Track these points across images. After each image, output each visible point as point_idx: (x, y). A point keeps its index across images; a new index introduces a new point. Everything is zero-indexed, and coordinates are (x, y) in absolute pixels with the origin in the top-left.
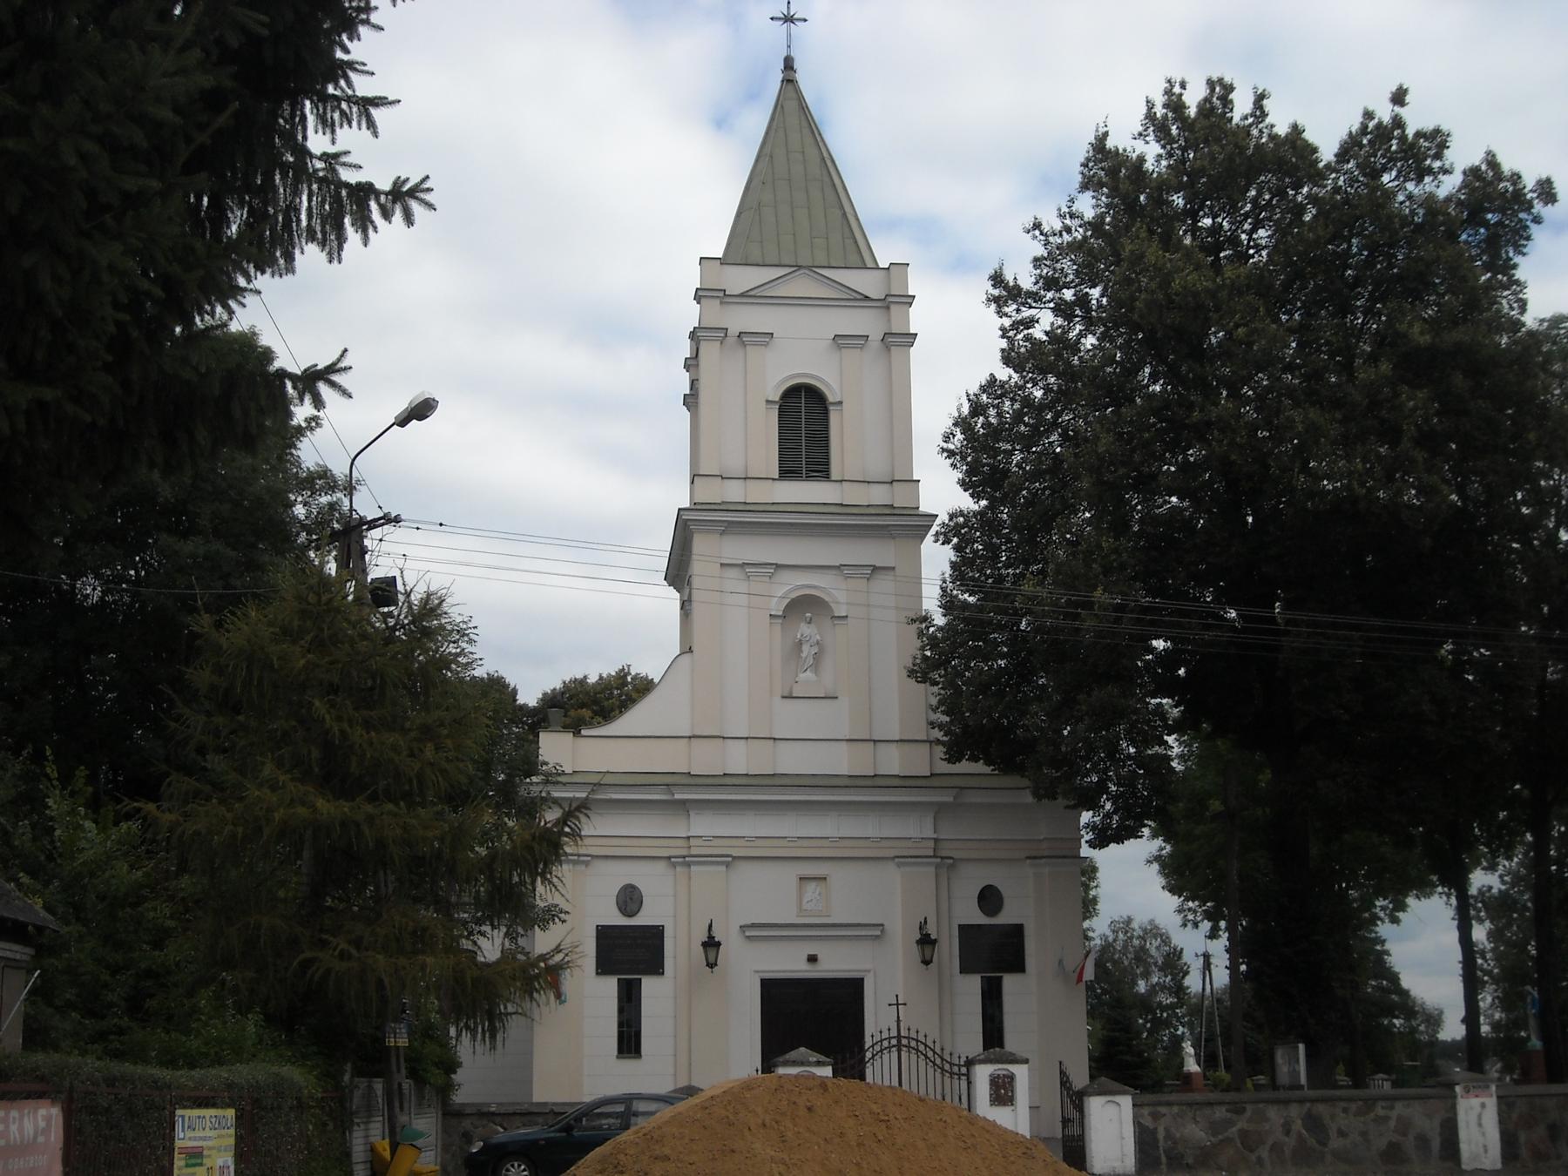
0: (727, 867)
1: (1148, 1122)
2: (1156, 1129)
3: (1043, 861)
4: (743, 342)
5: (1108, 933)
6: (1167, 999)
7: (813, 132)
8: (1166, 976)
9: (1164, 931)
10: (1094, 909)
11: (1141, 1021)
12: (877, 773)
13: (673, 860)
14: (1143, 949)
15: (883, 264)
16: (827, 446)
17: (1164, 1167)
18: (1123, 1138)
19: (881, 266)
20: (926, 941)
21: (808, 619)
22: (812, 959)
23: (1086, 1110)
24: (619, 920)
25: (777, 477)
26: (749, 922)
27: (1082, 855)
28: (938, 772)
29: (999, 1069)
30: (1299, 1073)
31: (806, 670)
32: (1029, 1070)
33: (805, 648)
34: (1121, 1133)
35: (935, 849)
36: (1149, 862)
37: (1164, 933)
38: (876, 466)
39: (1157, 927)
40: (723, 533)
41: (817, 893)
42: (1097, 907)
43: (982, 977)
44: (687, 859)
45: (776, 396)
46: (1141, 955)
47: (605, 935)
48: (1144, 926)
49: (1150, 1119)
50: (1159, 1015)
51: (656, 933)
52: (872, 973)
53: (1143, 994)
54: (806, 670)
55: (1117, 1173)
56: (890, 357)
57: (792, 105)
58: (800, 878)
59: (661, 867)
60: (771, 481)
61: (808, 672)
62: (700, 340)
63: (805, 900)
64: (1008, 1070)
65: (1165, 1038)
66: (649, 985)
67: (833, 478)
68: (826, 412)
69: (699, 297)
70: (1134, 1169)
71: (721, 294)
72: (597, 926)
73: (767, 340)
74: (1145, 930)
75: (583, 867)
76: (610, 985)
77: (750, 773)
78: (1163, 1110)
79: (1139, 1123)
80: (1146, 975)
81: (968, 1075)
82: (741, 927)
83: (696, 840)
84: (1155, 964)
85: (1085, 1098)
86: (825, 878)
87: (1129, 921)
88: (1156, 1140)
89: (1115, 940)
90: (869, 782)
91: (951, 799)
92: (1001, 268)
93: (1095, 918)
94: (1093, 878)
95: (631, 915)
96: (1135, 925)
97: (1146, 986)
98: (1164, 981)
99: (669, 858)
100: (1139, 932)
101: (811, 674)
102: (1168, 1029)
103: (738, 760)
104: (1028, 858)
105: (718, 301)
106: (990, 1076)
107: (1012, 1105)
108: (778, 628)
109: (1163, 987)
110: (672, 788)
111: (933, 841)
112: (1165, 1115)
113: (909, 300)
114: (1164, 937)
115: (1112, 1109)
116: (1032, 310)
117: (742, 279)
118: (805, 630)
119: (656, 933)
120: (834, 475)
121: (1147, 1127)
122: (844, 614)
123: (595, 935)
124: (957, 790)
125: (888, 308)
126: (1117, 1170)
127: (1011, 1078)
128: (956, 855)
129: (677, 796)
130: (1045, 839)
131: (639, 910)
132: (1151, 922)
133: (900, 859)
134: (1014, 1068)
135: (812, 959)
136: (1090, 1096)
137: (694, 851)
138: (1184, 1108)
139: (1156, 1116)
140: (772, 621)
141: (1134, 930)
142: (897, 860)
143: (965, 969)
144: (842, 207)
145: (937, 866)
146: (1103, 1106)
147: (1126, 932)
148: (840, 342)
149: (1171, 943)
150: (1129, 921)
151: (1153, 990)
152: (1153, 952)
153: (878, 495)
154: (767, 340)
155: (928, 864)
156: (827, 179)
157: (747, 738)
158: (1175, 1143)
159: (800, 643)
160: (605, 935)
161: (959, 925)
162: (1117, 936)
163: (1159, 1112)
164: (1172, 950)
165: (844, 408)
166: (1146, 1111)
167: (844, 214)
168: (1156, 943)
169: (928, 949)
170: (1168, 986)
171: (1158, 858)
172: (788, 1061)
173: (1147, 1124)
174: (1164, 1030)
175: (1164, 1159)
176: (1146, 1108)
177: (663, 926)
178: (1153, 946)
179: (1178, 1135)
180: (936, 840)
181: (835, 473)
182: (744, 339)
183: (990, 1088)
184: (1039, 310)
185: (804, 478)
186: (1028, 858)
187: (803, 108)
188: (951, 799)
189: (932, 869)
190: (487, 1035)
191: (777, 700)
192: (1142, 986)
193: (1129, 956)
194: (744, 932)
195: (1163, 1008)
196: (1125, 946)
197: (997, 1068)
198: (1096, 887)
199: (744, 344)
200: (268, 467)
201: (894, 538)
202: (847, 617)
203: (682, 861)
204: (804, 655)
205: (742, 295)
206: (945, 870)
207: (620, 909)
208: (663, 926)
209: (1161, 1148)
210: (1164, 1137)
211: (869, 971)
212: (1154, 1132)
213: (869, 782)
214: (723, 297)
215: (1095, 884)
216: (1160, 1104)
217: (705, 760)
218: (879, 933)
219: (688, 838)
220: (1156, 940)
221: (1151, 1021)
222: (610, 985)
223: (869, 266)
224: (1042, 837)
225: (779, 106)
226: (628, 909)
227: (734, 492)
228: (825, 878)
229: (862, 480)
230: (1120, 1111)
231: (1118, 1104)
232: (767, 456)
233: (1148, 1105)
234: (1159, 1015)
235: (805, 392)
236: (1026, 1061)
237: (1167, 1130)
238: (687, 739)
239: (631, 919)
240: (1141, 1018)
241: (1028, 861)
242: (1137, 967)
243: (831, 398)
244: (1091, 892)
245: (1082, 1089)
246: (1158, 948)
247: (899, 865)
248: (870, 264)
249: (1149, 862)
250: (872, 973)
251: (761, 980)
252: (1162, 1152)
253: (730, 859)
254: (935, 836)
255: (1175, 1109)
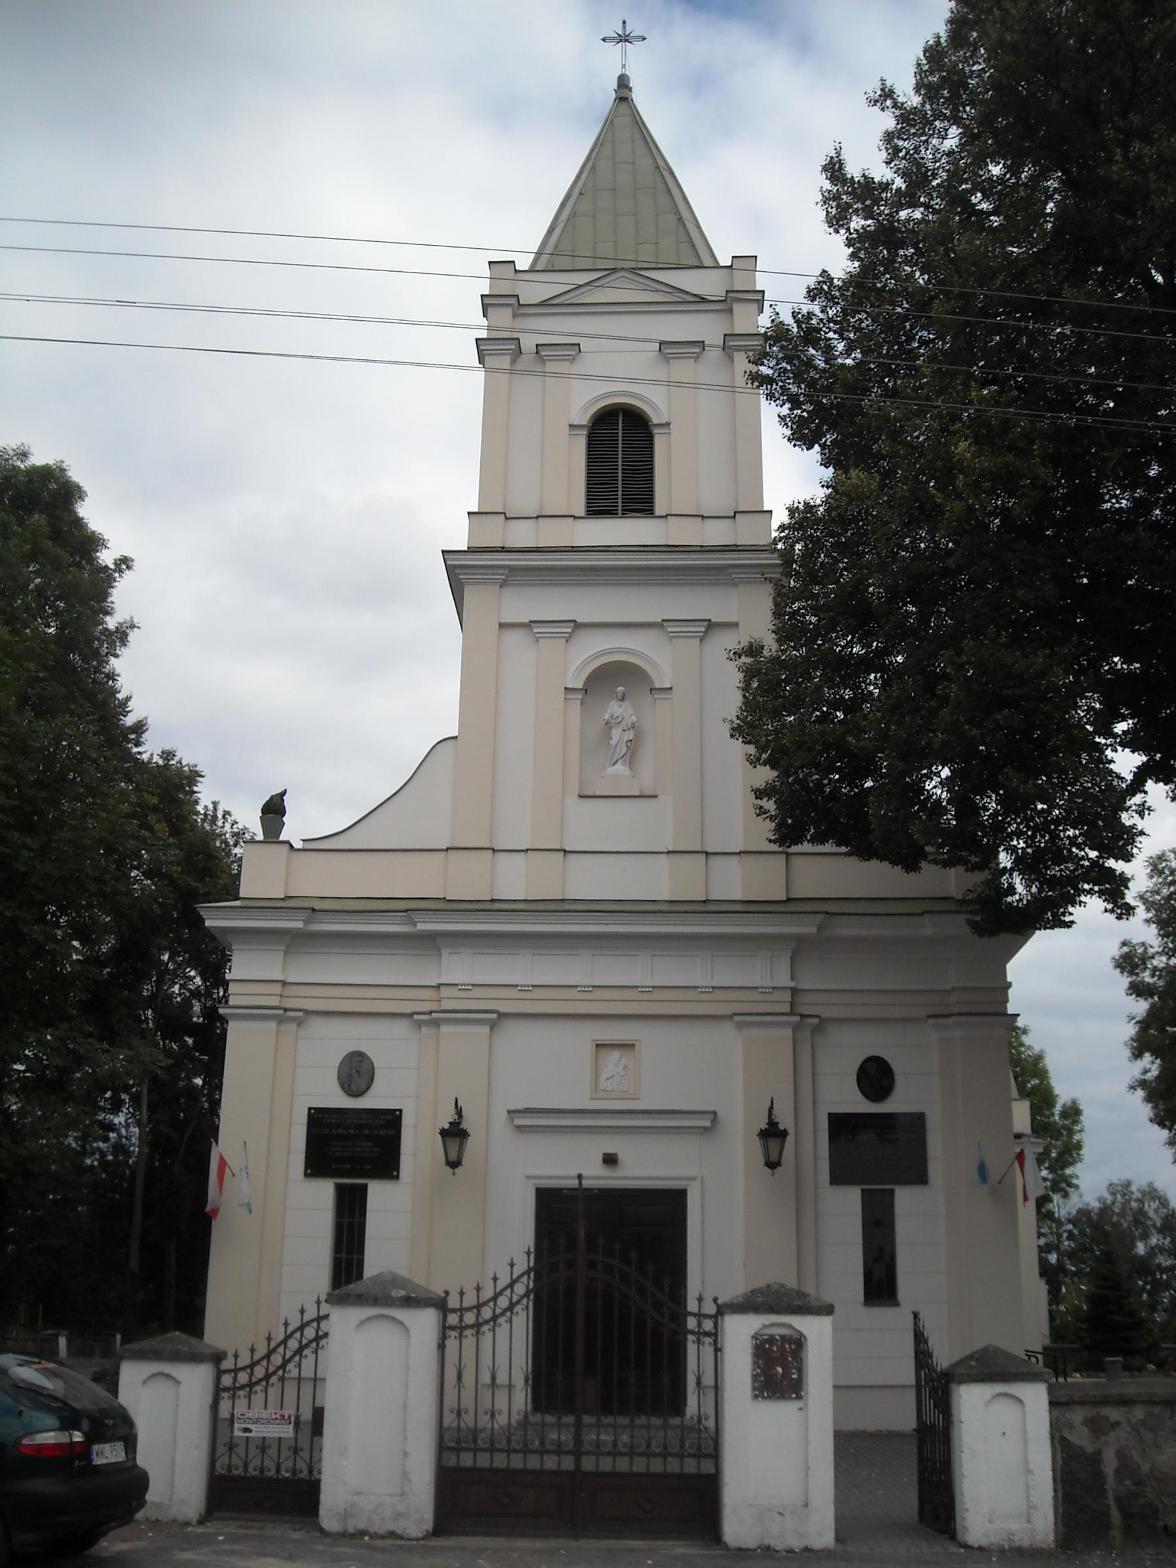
0: (491, 1028)
1: (1081, 1437)
2: (1099, 1452)
3: (951, 1021)
4: (541, 356)
5: (1107, 1195)
6: (1166, 1261)
7: (647, 144)
8: (1165, 1238)
9: (1162, 1193)
10: (1078, 1154)
11: (1140, 1283)
12: (709, 898)
13: (415, 1017)
14: (1141, 1212)
15: (725, 261)
16: (651, 480)
17: (1116, 1534)
18: (1029, 1472)
19: (722, 265)
20: (772, 1133)
21: (620, 695)
22: (610, 1160)
23: (954, 1411)
24: (339, 1100)
25: (582, 513)
26: (521, 1106)
27: (1010, 1012)
28: (796, 897)
29: (773, 1325)
30: (1090, 1382)
31: (616, 762)
32: (835, 1330)
33: (616, 734)
34: (1026, 1461)
35: (792, 1004)
36: (1133, 1088)
37: (1162, 1196)
38: (715, 499)
39: (1155, 1190)
40: (503, 584)
41: (622, 1066)
42: (1082, 1152)
43: (862, 1190)
44: (434, 1015)
45: (585, 419)
46: (1139, 1217)
47: (319, 1120)
48: (1142, 1188)
49: (1085, 1431)
50: (1158, 1277)
51: (391, 1120)
52: (699, 1180)
53: (1142, 1256)
54: (616, 762)
55: (1018, 1543)
56: (733, 366)
57: (624, 121)
58: (597, 1045)
59: (401, 1028)
60: (572, 518)
61: (618, 765)
62: (485, 355)
63: (604, 1076)
64: (790, 1327)
65: (1165, 1300)
66: (378, 1192)
67: (657, 514)
68: (651, 437)
69: (488, 303)
70: (1052, 1537)
71: (513, 301)
72: (310, 1109)
73: (572, 353)
74: (1144, 1193)
75: (293, 1026)
76: (324, 1191)
77: (528, 899)
78: (1113, 1413)
79: (1063, 1440)
80: (1145, 1237)
81: (715, 1335)
82: (509, 1112)
83: (453, 992)
84: (1154, 1226)
85: (954, 1387)
86: (633, 1045)
87: (1128, 1184)
88: (1099, 1476)
89: (1113, 1203)
90: (702, 908)
91: (814, 930)
92: (838, 154)
93: (1079, 1164)
94: (1076, 1122)
96: (1134, 1188)
97: (1145, 1248)
98: (1164, 1244)
99: (412, 1014)
100: (1137, 1195)
101: (622, 767)
102: (1169, 1291)
104: (930, 1016)
105: (509, 311)
106: (755, 1337)
107: (799, 1397)
108: (575, 707)
109: (1162, 1249)
110: (414, 915)
111: (790, 992)
112: (1117, 1424)
113: (759, 297)
114: (1162, 1200)
115: (1005, 1412)
118: (615, 708)
119: (391, 1120)
120: (659, 509)
121: (1081, 1448)
122: (668, 686)
123: (305, 1121)
124: (823, 916)
125: (731, 311)
126: (1016, 1539)
127: (798, 1343)
128: (826, 1013)
129: (420, 927)
130: (954, 989)
131: (368, 1088)
132: (1150, 1184)
133: (739, 1019)
134: (802, 1323)
135: (610, 1160)
136: (960, 1383)
137: (446, 1005)
138: (1157, 1410)
139: (1097, 1427)
140: (569, 696)
141: (1132, 1193)
142: (736, 1018)
143: (837, 1179)
144: (677, 212)
145: (796, 1029)
146: (986, 1405)
147: (1125, 1194)
148: (667, 351)
149: (1168, 1205)
150: (1128, 1184)
151: (1153, 1251)
152: (1152, 1214)
153: (716, 534)
154: (572, 353)
155: (786, 1024)
156: (661, 186)
157: (527, 850)
158: (1139, 1483)
160: (319, 1120)
161: (829, 1114)
162: (1115, 1199)
163: (1107, 1418)
164: (1170, 1212)
165: (672, 432)
166: (1077, 1416)
167: (680, 219)
168: (1155, 1205)
169: (774, 1145)
170: (1167, 1248)
171: (1143, 1084)
172: (348, 1295)
173: (1079, 1443)
174: (1165, 1292)
175: (1116, 1516)
176: (1078, 1408)
177: (401, 1111)
178: (1151, 1208)
179: (1145, 1468)
180: (794, 991)
181: (660, 507)
182: (543, 353)
183: (754, 1363)
185: (620, 515)
186: (930, 1016)
187: (637, 123)
188: (813, 930)
189: (788, 1033)
191: (572, 799)
192: (1141, 1248)
193: (1127, 1218)
194: (512, 1120)
195: (1163, 1270)
196: (1123, 1209)
197: (767, 1323)
198: (1080, 1131)
199: (543, 361)
201: (736, 585)
202: (671, 688)
204: (613, 742)
205: (542, 304)
206: (808, 1034)
207: (342, 1086)
208: (401, 1111)
209: (1110, 1495)
210: (1117, 1471)
211: (694, 1179)
212: (1095, 1459)
213: (702, 908)
214: (519, 308)
215: (1079, 1129)
216: (1107, 1401)
218: (708, 1123)
219: (439, 986)
220: (1155, 1202)
221: (1151, 1283)
222: (324, 1191)
223: (705, 265)
224: (949, 987)
225: (609, 123)
226: (353, 1086)
227: (522, 535)
228: (633, 1045)
229: (695, 513)
230: (1024, 1412)
231: (1020, 1401)
233: (1081, 1403)
234: (1158, 1277)
235: (623, 416)
236: (828, 1310)
237: (1122, 1456)
238: (443, 854)
240: (1141, 1280)
241: (931, 1021)
242: (1136, 1229)
243: (655, 420)
244: (1075, 1137)
245: (948, 1368)
246: (1156, 1211)
247: (740, 1026)
248: (707, 262)
249: (1133, 1088)
250: (699, 1180)
251: (538, 1190)
252: (1111, 1501)
253: (495, 1016)
254: (792, 984)
255: (1139, 1413)
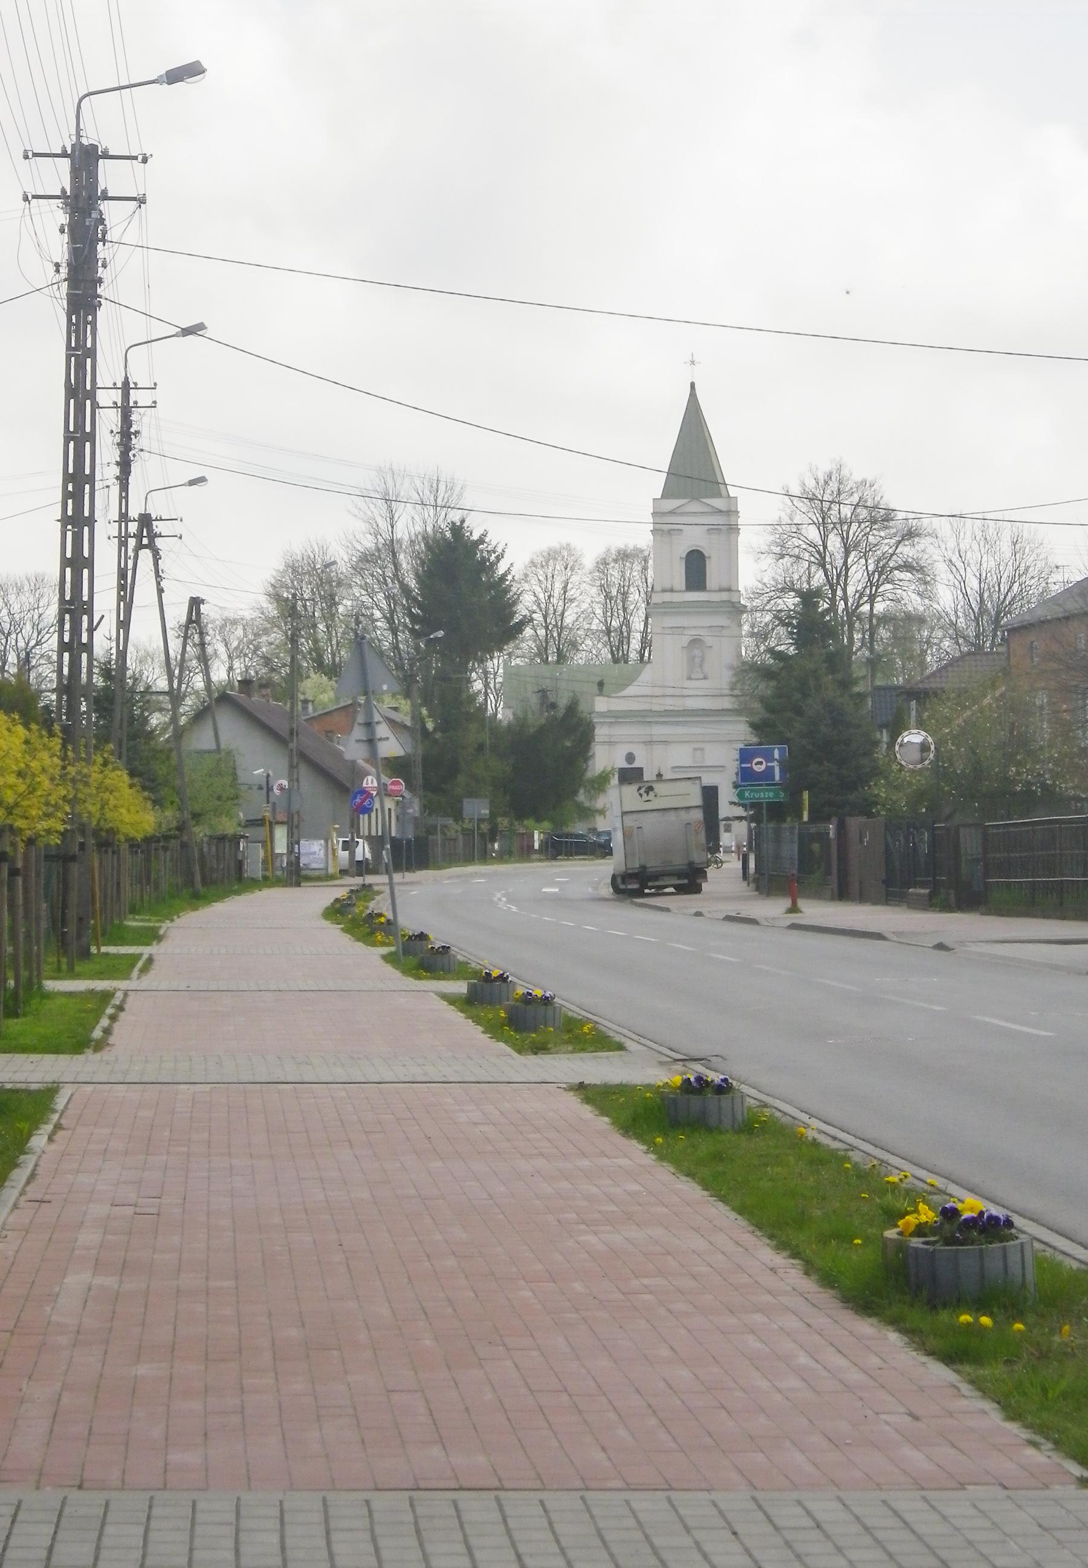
45: (684, 555)
51: (640, 770)
95: (631, 764)
103: (670, 704)
116: (881, 1157)
117: (672, 504)
119: (640, 770)
122: (581, 1502)
159: (695, 657)
184: (938, 1551)
190: (635, 644)
200: (411, 626)
203: (649, 743)
217: (657, 705)
232: (680, 581)
239: (532, 1060)
243: (706, 555)
